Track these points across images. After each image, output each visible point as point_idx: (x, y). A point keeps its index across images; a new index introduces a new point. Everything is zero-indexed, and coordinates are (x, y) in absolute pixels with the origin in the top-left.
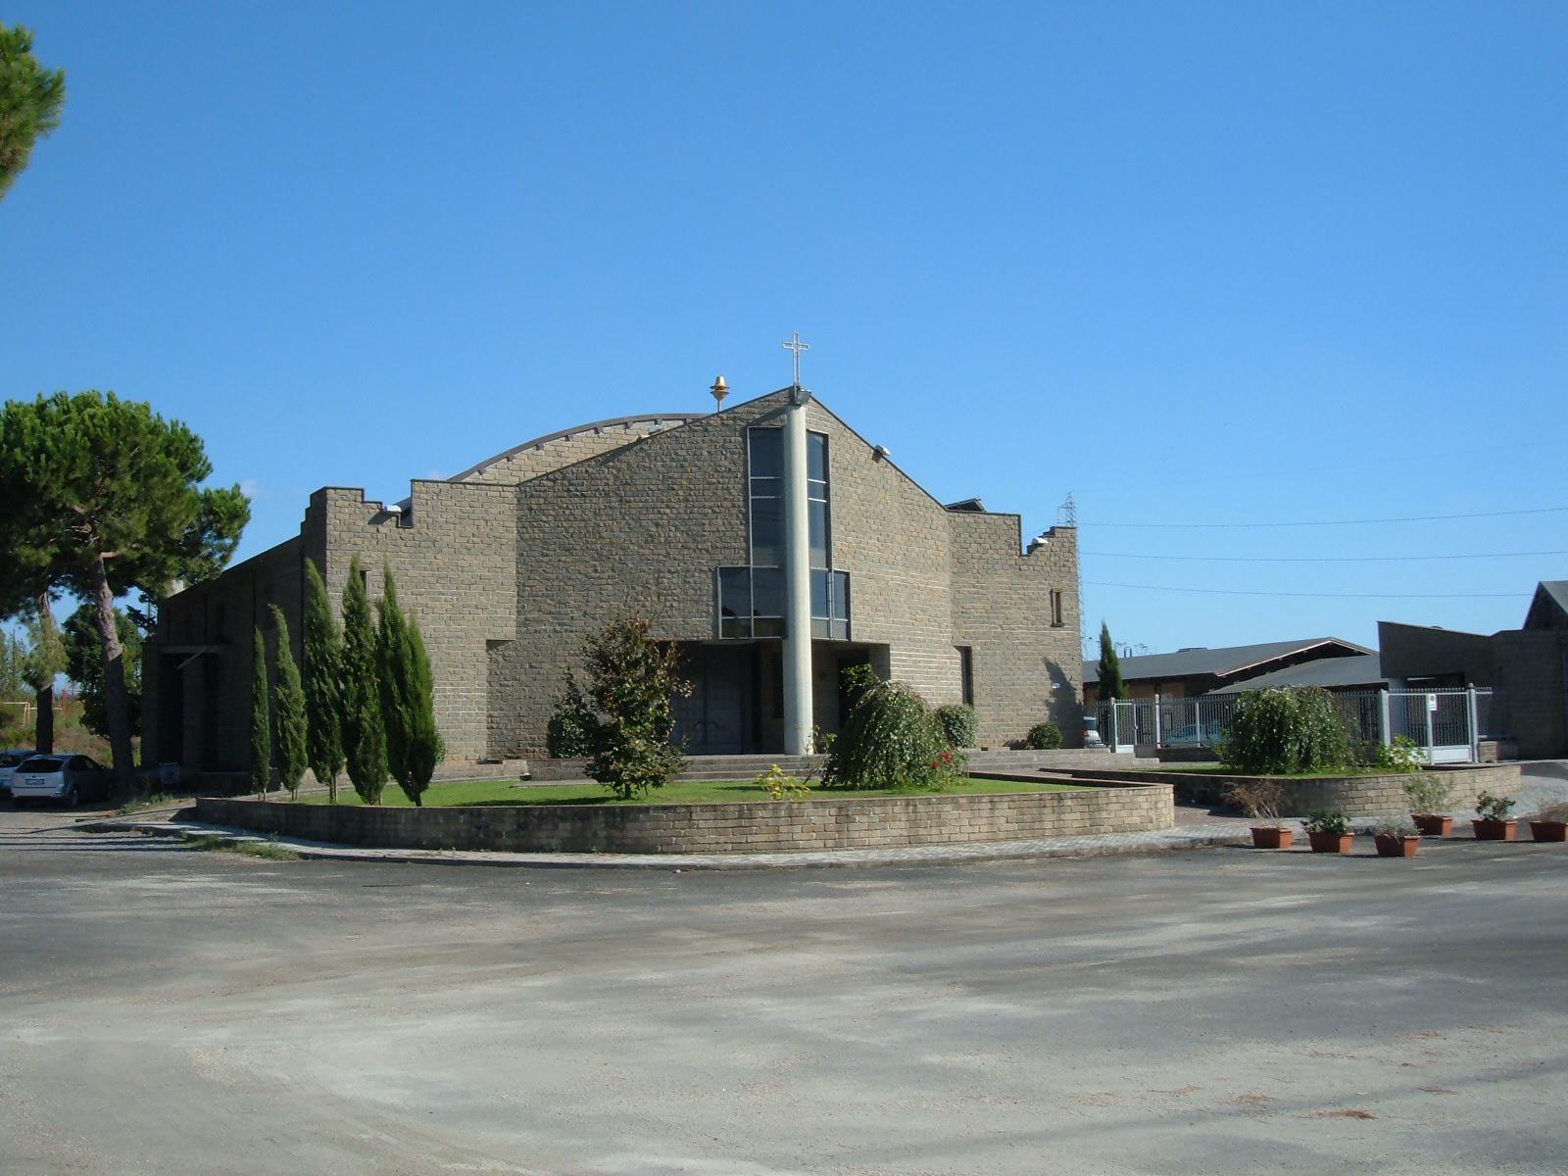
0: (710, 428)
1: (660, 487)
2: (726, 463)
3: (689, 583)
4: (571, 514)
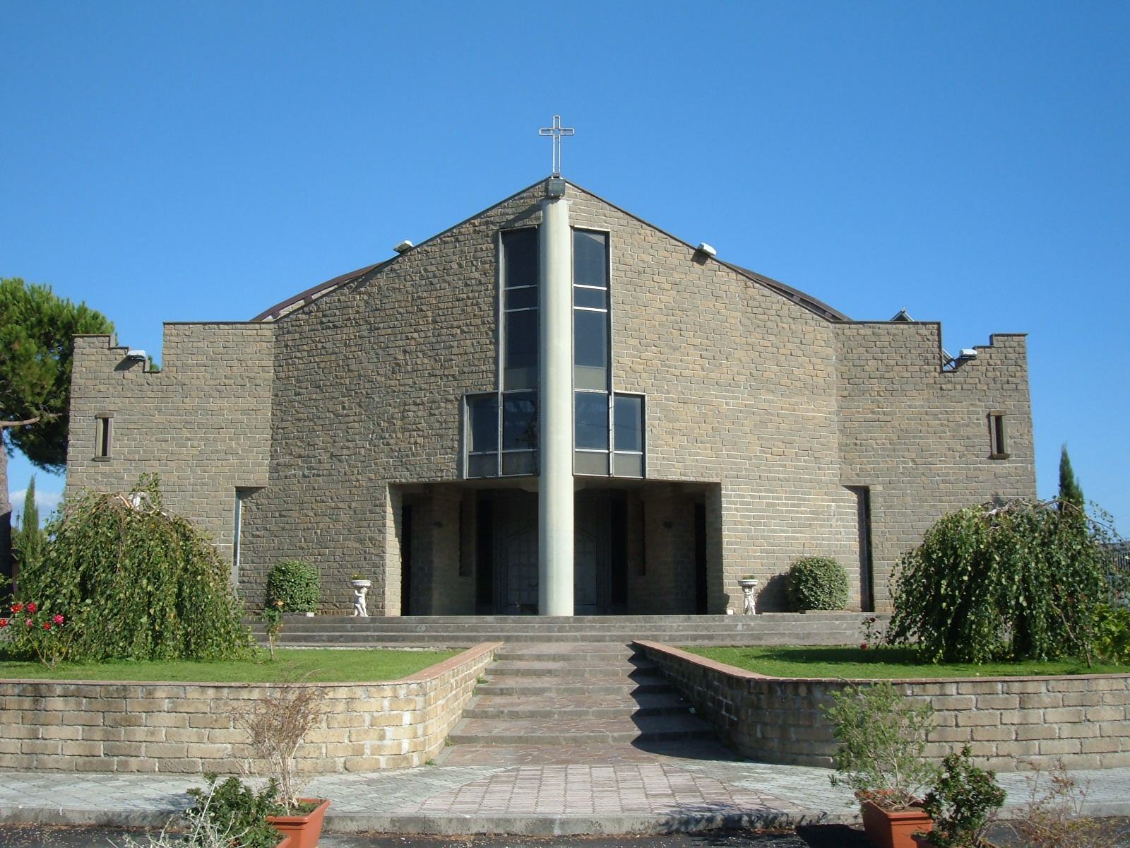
0: (461, 238)
1: (410, 309)
2: (477, 275)
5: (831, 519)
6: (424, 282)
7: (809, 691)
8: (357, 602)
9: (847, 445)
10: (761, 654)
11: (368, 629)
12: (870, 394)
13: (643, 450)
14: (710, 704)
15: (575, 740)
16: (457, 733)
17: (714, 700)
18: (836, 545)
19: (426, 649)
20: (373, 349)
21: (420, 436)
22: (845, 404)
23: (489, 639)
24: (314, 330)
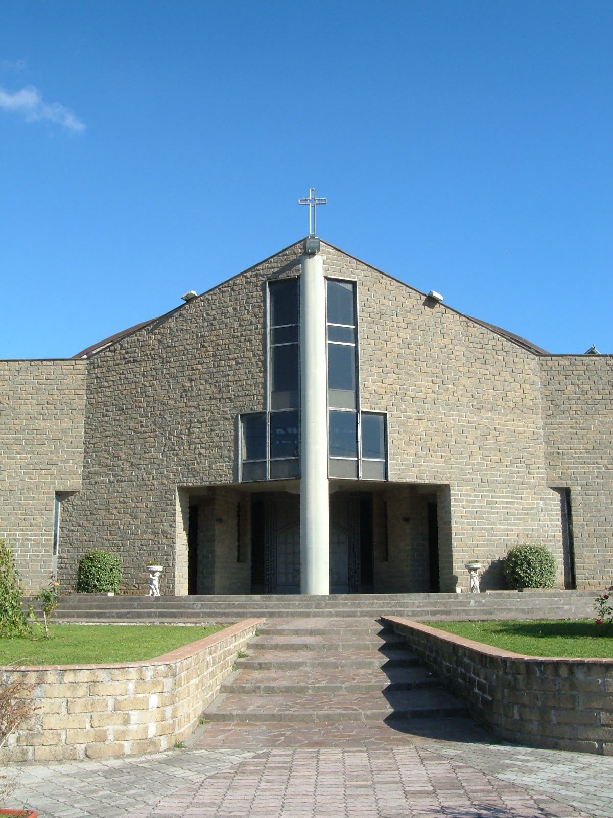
0: (236, 288)
1: (195, 346)
2: (249, 317)
3: (215, 431)
4: (126, 378)
5: (540, 514)
6: (206, 324)
7: (571, 673)
8: (151, 583)
9: (551, 454)
10: (498, 628)
12: (569, 413)
13: (386, 458)
14: (460, 681)
15: (328, 717)
16: (213, 710)
17: (464, 677)
18: (544, 535)
19: (198, 625)
20: (165, 378)
21: (203, 448)
22: (549, 421)
23: (255, 615)
24: (118, 364)
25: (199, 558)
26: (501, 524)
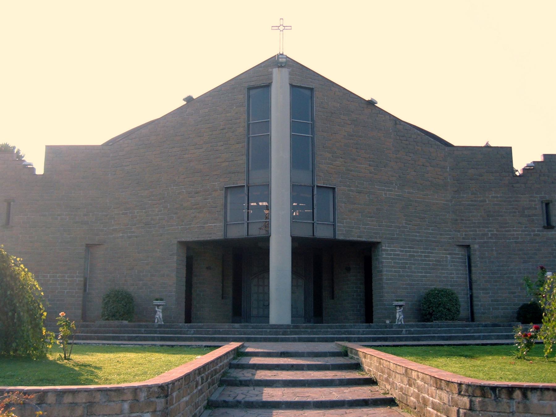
7: (525, 396)
11: (155, 332)
18: (451, 281)
25: (194, 295)
26: (419, 272)
